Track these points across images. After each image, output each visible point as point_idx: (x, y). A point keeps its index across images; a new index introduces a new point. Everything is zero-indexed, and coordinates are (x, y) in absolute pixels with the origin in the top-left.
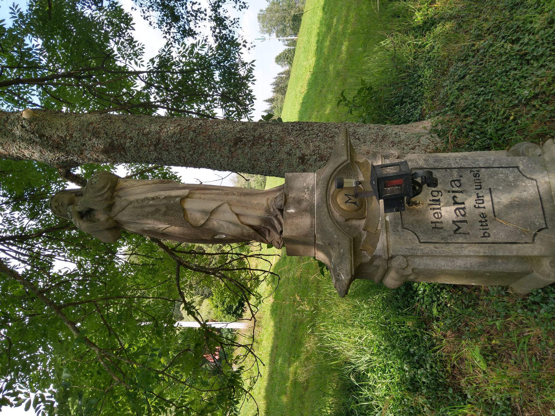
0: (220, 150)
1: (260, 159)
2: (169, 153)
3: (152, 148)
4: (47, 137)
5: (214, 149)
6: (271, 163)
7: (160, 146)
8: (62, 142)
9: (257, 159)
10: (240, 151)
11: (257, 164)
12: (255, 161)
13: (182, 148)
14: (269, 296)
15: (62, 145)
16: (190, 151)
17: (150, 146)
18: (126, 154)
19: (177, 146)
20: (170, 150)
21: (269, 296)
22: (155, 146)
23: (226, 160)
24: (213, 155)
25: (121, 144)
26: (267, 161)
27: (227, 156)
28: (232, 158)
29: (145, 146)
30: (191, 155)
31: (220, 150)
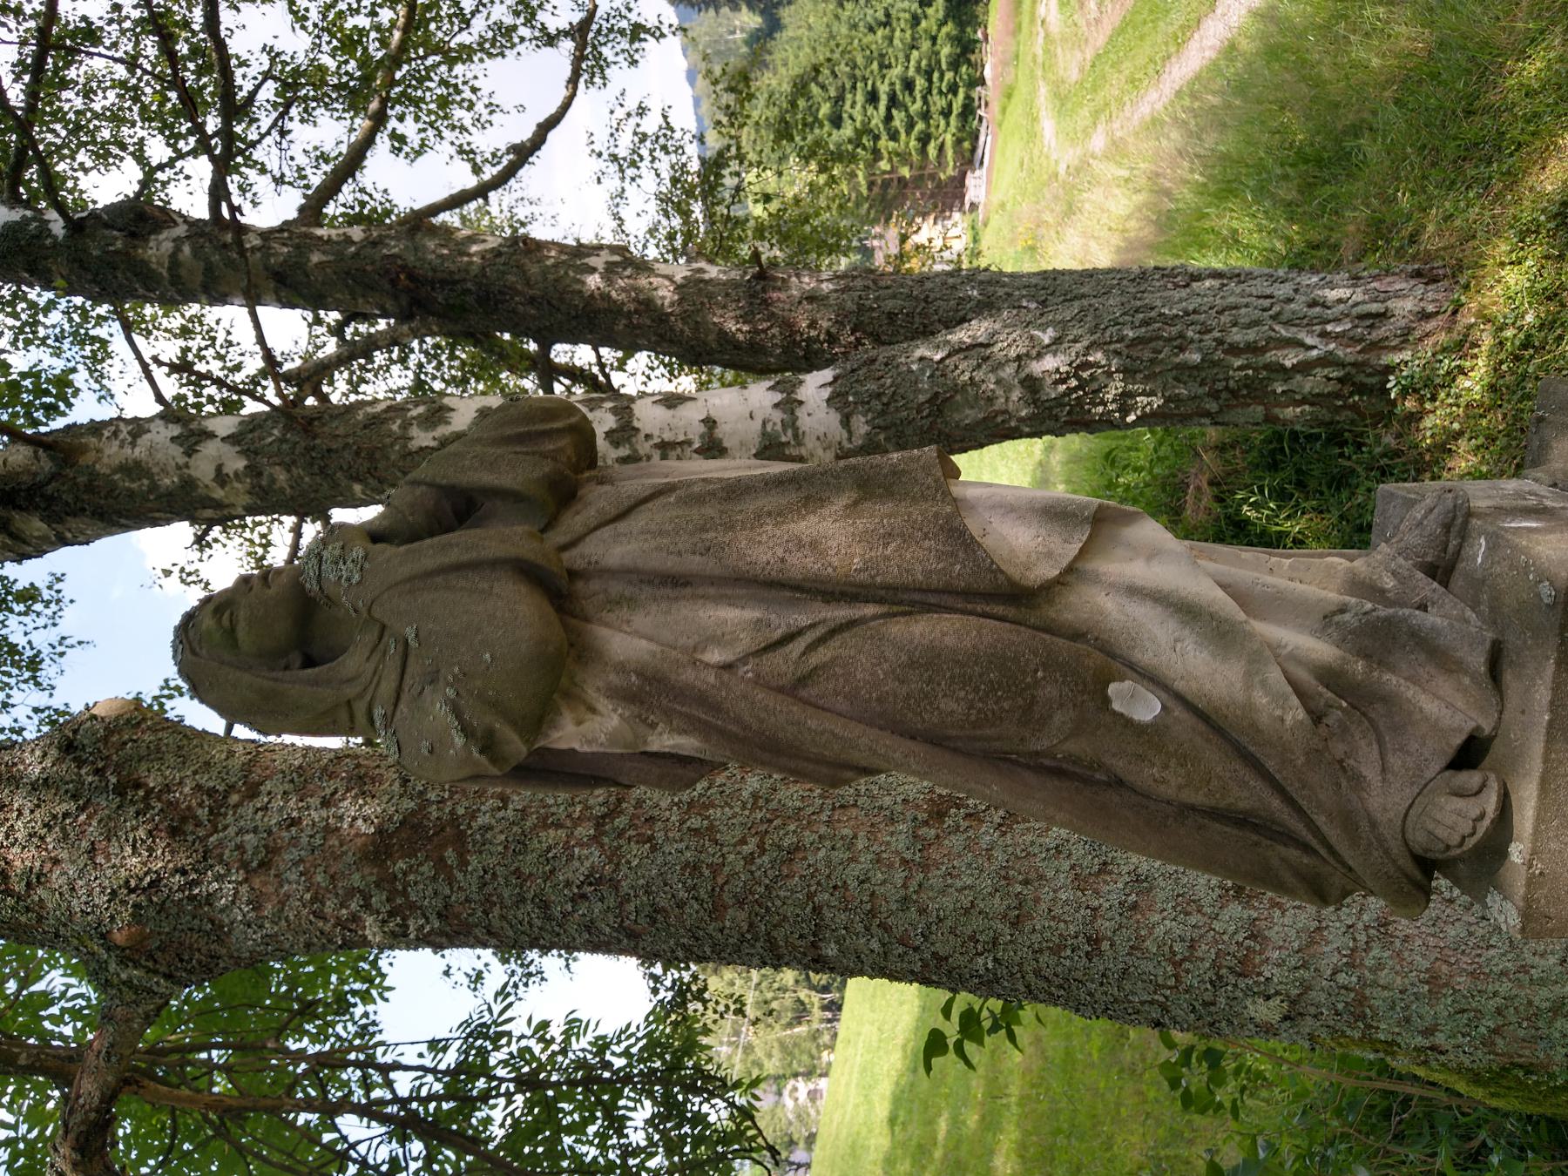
0: (872, 835)
1: (1050, 874)
2: (654, 849)
3: (585, 831)
4: (149, 792)
5: (846, 831)
6: (1096, 892)
7: (621, 822)
8: (203, 813)
9: (1033, 875)
10: (956, 842)
11: (1037, 900)
12: (1026, 882)
13: (711, 828)
14: (253, 94)
15: (198, 824)
16: (743, 842)
17: (577, 822)
18: (463, 863)
19: (695, 822)
20: (660, 836)
21: (253, 94)
22: (600, 822)
23: (899, 876)
24: (841, 855)
25: (454, 819)
26: (1080, 881)
27: (904, 862)
28: (925, 867)
29: (558, 825)
30: (749, 859)
31: (872, 835)
